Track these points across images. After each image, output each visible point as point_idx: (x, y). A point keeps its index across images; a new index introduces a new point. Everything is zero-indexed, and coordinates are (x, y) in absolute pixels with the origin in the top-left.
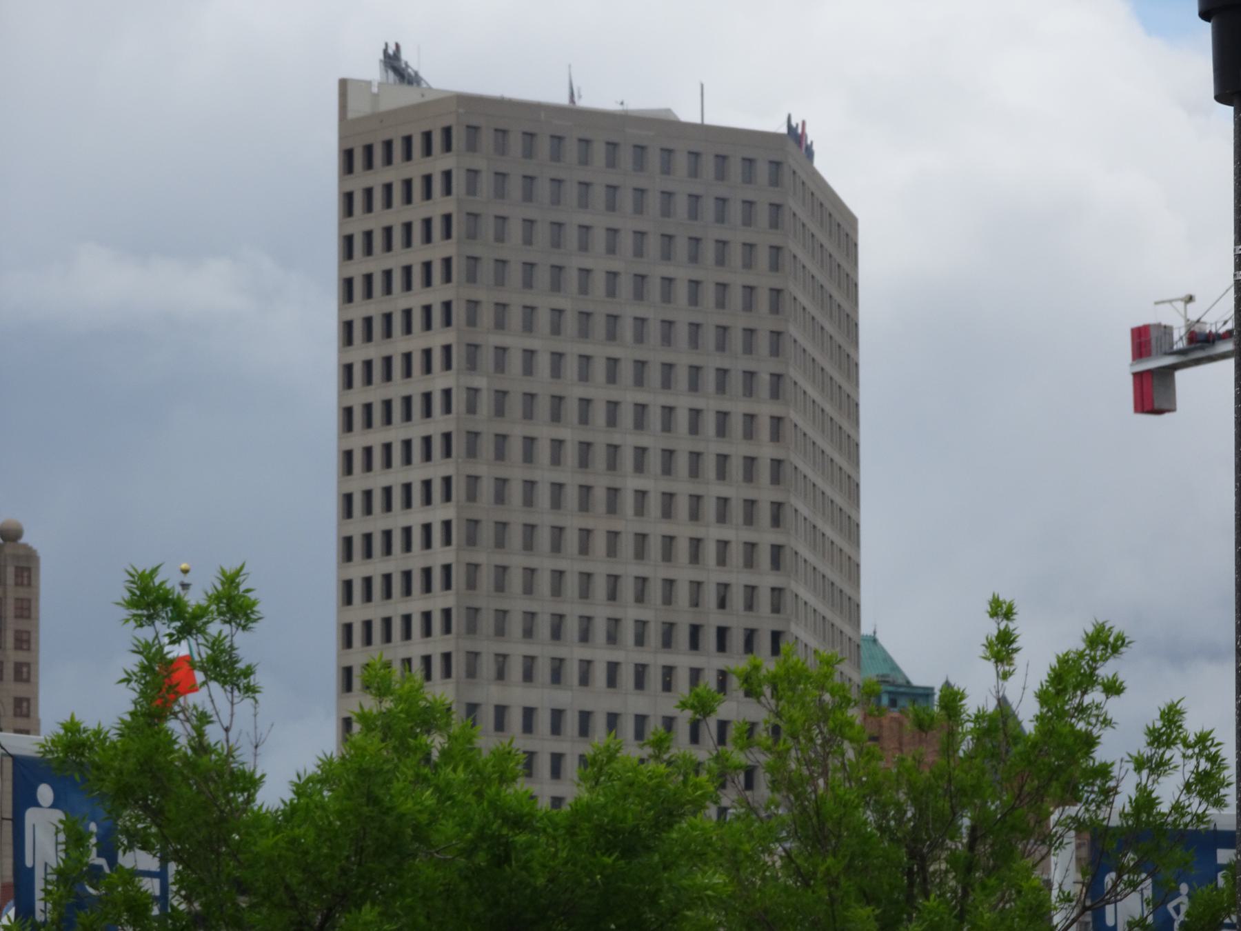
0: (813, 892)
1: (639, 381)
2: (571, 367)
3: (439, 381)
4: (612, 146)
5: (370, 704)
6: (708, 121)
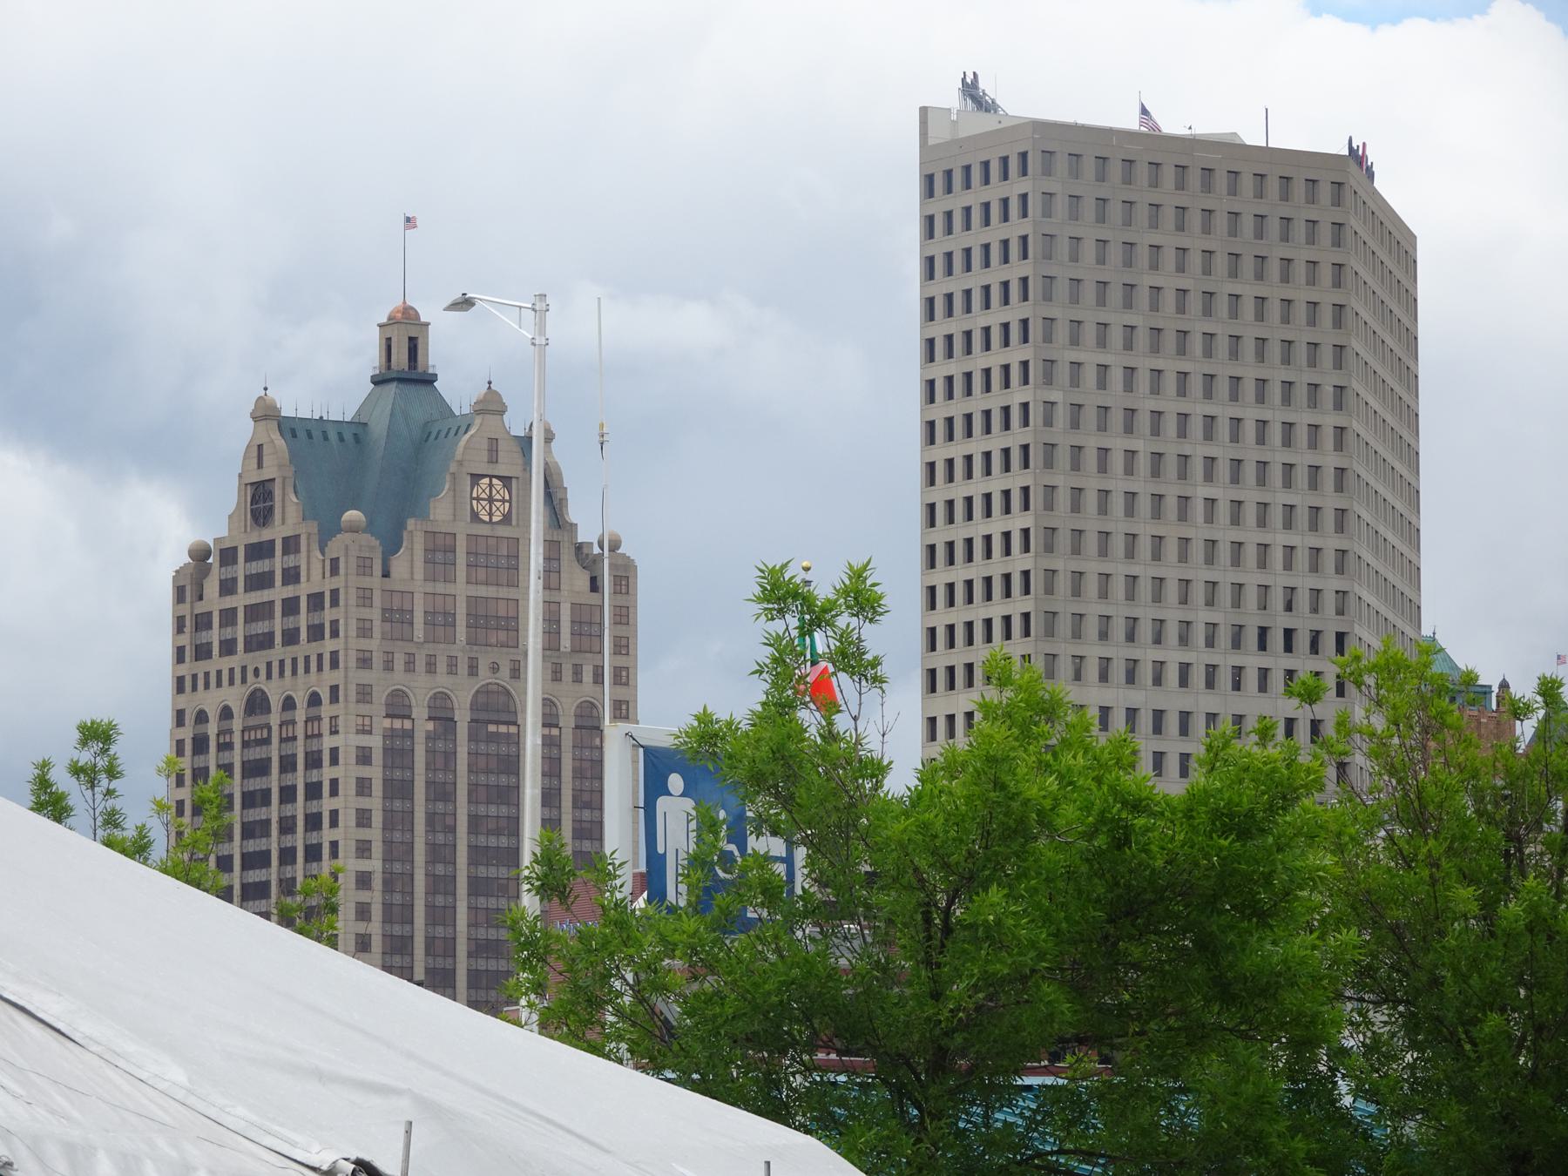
0: (1415, 874)
2: (1143, 381)
3: (1018, 395)
5: (992, 694)
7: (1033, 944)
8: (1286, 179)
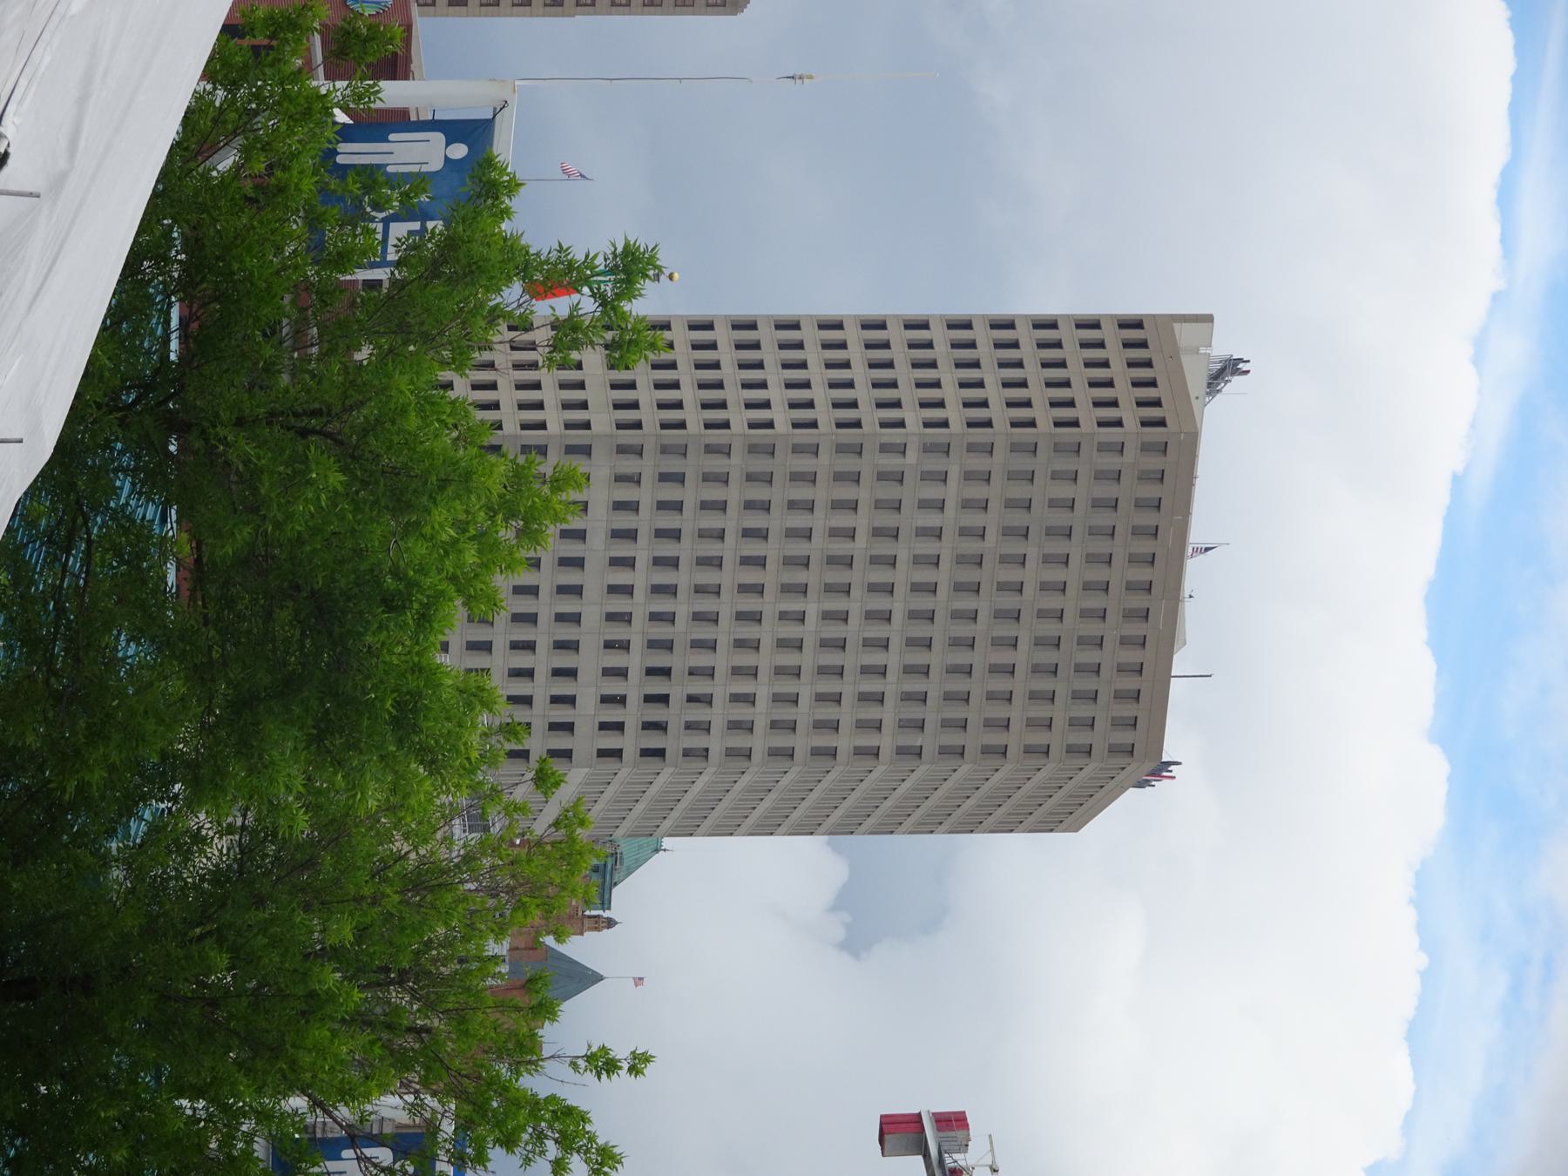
0: (366, 882)
1: (914, 615)
2: (927, 547)
3: (912, 416)
4: (1148, 588)
6: (1175, 684)
7: (290, 517)
8: (1136, 696)
